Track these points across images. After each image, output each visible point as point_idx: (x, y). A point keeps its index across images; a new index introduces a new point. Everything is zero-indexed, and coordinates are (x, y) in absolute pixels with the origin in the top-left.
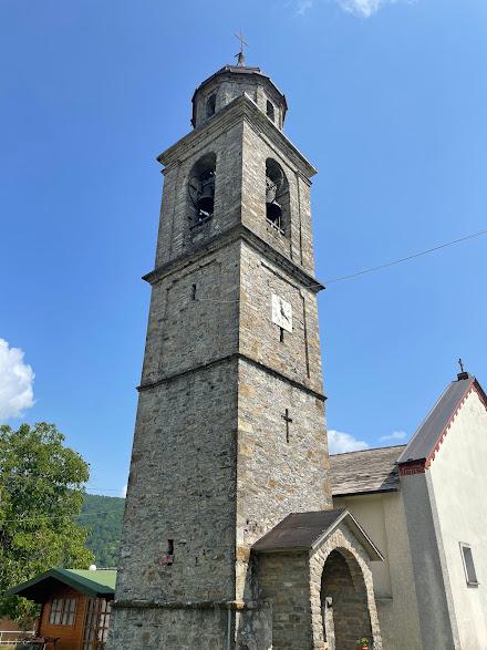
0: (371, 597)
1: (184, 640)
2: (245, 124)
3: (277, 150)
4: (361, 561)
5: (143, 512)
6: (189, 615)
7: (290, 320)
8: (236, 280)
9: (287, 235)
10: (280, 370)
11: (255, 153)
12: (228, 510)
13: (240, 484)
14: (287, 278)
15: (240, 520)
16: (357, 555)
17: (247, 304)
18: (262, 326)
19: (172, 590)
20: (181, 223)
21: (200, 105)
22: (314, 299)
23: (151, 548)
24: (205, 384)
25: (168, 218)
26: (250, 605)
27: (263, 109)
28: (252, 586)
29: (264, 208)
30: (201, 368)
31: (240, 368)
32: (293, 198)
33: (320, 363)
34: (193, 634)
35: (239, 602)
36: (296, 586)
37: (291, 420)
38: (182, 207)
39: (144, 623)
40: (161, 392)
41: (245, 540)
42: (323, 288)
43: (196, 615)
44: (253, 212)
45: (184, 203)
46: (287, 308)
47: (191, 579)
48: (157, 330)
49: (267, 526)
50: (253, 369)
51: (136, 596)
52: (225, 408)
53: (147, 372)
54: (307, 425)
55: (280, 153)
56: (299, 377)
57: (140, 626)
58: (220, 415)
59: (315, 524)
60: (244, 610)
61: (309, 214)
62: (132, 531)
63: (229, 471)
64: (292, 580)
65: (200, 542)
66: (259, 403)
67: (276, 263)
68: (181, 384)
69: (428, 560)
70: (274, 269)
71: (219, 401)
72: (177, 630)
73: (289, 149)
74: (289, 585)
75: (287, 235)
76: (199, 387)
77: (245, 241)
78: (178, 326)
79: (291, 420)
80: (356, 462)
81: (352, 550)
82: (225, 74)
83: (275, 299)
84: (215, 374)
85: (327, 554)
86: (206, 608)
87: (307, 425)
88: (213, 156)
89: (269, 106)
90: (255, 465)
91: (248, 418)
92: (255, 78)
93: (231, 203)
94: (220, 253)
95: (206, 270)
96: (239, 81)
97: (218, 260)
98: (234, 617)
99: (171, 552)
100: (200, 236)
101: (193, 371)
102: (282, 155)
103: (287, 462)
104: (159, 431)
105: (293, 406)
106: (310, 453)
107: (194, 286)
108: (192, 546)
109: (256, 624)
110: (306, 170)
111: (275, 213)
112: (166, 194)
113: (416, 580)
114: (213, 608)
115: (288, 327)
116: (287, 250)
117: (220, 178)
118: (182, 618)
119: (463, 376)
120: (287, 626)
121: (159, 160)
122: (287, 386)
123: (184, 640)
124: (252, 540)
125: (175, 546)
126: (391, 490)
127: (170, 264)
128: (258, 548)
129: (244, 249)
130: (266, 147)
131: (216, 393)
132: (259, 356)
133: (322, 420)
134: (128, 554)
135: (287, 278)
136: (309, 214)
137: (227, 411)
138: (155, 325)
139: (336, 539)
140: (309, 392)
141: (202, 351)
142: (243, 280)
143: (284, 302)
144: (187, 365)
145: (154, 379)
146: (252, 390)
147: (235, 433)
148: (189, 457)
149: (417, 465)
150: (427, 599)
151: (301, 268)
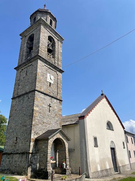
0: (67, 150)
1: (18, 161)
2: (42, 26)
3: (52, 33)
4: (65, 141)
5: (11, 131)
6: (19, 155)
7: (53, 81)
8: (36, 70)
9: (54, 57)
10: (48, 94)
11: (44, 35)
12: (30, 129)
13: (33, 123)
14: (53, 69)
15: (33, 132)
16: (63, 140)
17: (39, 76)
18: (44, 82)
19: (16, 149)
20: (25, 54)
21: (32, 20)
22: (61, 75)
23: (12, 139)
24: (27, 98)
25: (21, 52)
26: (34, 152)
27: (48, 22)
28: (35, 148)
29: (47, 50)
30: (26, 93)
31: (36, 94)
32: (56, 47)
33: (62, 92)
34: (20, 160)
35: (31, 151)
36: (45, 147)
37: (51, 107)
38: (25, 49)
39: (10, 158)
40: (17, 100)
41: (33, 137)
42: (64, 72)
43: (21, 155)
44: (43, 51)
45: (26, 48)
46: (52, 77)
47: (21, 146)
48: (17, 83)
49: (41, 133)
50: (40, 94)
51: (8, 151)
52: (31, 104)
53: (14, 94)
54: (56, 108)
55: (53, 34)
56: (55, 95)
57: (9, 158)
58: (30, 106)
59: (51, 132)
60: (32, 153)
61: (61, 51)
62: (8, 135)
63: (31, 120)
64: (44, 146)
65: (23, 137)
66: (40, 102)
67: (49, 65)
68: (22, 98)
69: (83, 140)
70: (49, 67)
71: (30, 102)
72: (16, 159)
73: (56, 33)
74: (44, 147)
75: (54, 57)
76: (26, 98)
77: (39, 59)
78: (22, 82)
79: (51, 107)
80: (68, 117)
81: (62, 138)
82: (38, 11)
83: (48, 75)
84: (30, 95)
85: (54, 140)
86: (23, 153)
87: (56, 108)
88: (33, 35)
89: (51, 20)
90: (38, 118)
91: (37, 106)
92: (46, 13)
93: (37, 49)
94: (33, 62)
95: (30, 67)
96: (42, 13)
97: (33, 64)
98: (29, 155)
99: (17, 140)
100: (29, 57)
101: (25, 94)
102: (54, 35)
103: (46, 117)
104: (16, 110)
105: (52, 103)
106: (56, 115)
107: (27, 71)
108: (21, 139)
109: (36, 157)
110: (61, 39)
111: (51, 51)
112: (21, 45)
113: (80, 145)
114: (25, 153)
115: (52, 82)
116: (53, 61)
117: (35, 42)
118: (18, 156)
119: (102, 95)
120: (42, 157)
121: (20, 35)
122: (50, 98)
123: (18, 161)
124: (36, 137)
125: (18, 138)
126: (77, 124)
127: (21, 65)
128: (37, 138)
129: (39, 61)
130: (49, 33)
131: (30, 100)
132: (42, 90)
133: (61, 106)
134: (7, 141)
135: (53, 69)
136: (61, 51)
137: (32, 104)
138: (17, 82)
139: (59, 136)
140: (57, 99)
141: (27, 89)
142: (38, 70)
143: (51, 76)
144: (24, 92)
145: (16, 96)
146: (39, 99)
147: (33, 110)
148: (22, 116)
149: (82, 117)
150: (82, 150)
151: (58, 67)
